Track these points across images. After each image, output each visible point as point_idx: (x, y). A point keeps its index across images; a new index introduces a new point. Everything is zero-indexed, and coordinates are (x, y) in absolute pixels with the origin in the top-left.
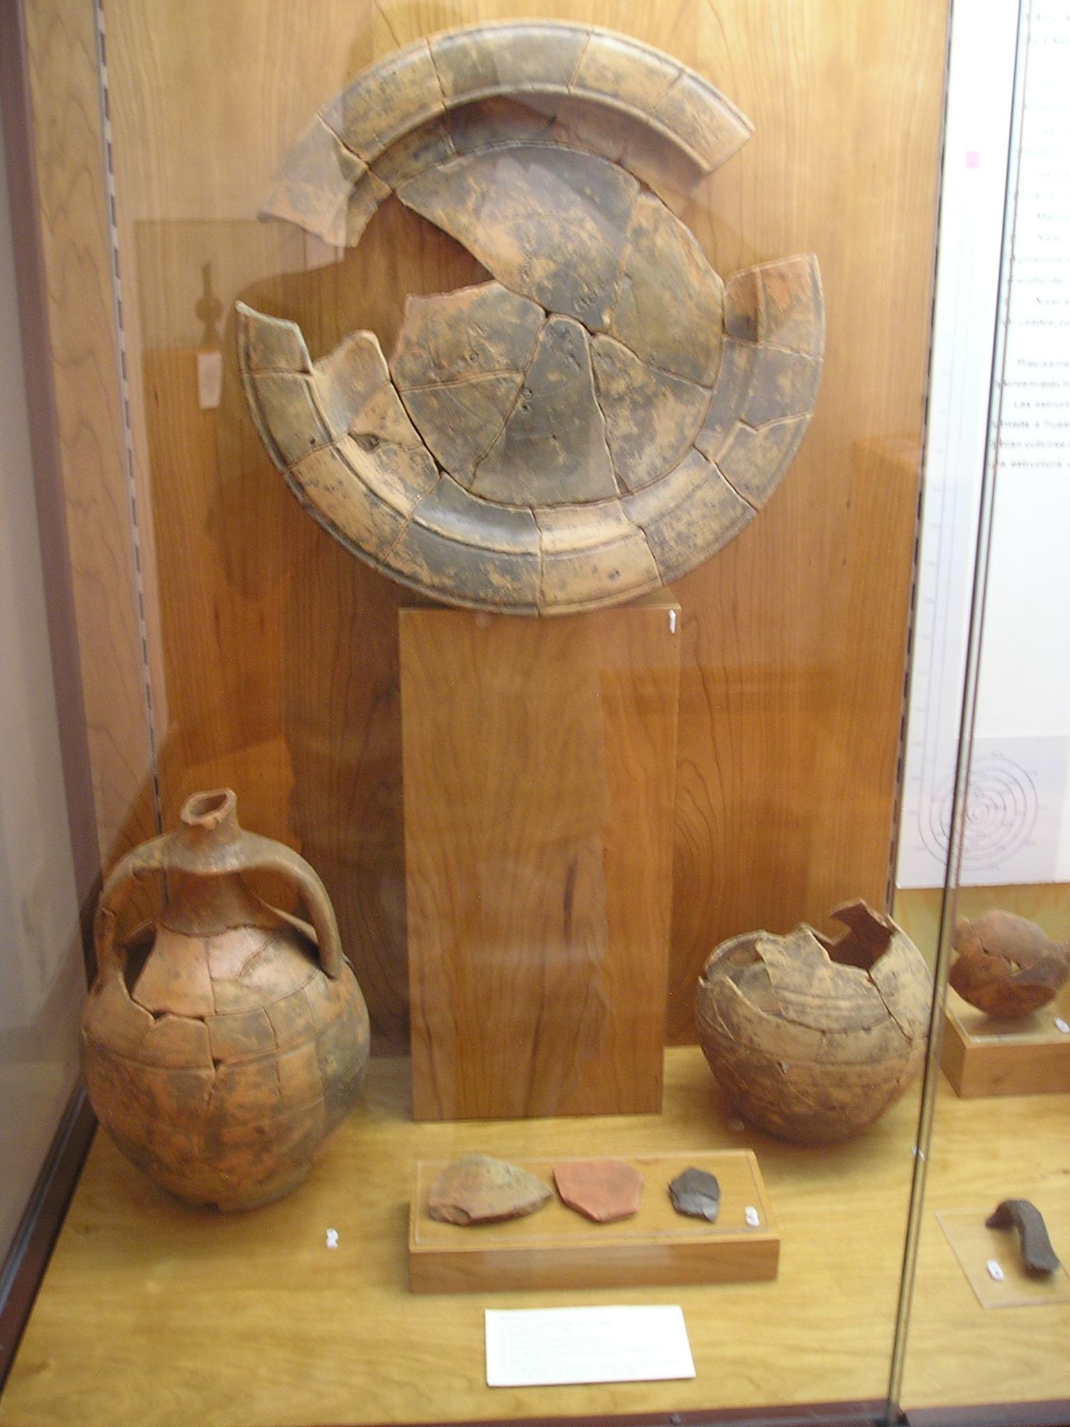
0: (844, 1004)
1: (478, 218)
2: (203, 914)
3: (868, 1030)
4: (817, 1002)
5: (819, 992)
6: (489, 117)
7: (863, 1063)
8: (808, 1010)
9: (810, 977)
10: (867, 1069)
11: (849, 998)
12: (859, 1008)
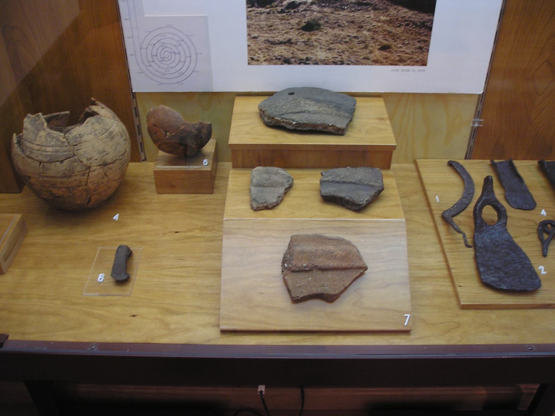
0: (49, 149)
1: (202, 136)
2: (540, 228)
3: (62, 162)
4: (38, 147)
5: (38, 143)
6: (252, 208)
7: (61, 177)
8: (33, 151)
9: (37, 135)
10: (65, 180)
11: (52, 146)
12: (57, 151)
